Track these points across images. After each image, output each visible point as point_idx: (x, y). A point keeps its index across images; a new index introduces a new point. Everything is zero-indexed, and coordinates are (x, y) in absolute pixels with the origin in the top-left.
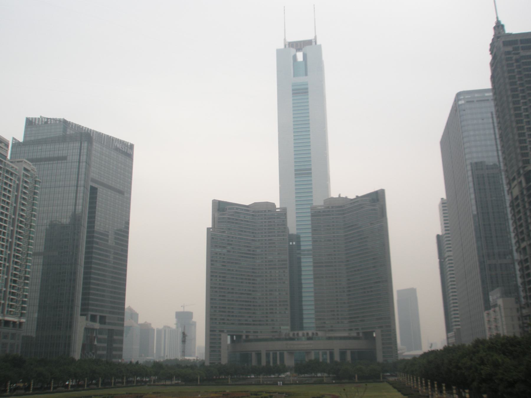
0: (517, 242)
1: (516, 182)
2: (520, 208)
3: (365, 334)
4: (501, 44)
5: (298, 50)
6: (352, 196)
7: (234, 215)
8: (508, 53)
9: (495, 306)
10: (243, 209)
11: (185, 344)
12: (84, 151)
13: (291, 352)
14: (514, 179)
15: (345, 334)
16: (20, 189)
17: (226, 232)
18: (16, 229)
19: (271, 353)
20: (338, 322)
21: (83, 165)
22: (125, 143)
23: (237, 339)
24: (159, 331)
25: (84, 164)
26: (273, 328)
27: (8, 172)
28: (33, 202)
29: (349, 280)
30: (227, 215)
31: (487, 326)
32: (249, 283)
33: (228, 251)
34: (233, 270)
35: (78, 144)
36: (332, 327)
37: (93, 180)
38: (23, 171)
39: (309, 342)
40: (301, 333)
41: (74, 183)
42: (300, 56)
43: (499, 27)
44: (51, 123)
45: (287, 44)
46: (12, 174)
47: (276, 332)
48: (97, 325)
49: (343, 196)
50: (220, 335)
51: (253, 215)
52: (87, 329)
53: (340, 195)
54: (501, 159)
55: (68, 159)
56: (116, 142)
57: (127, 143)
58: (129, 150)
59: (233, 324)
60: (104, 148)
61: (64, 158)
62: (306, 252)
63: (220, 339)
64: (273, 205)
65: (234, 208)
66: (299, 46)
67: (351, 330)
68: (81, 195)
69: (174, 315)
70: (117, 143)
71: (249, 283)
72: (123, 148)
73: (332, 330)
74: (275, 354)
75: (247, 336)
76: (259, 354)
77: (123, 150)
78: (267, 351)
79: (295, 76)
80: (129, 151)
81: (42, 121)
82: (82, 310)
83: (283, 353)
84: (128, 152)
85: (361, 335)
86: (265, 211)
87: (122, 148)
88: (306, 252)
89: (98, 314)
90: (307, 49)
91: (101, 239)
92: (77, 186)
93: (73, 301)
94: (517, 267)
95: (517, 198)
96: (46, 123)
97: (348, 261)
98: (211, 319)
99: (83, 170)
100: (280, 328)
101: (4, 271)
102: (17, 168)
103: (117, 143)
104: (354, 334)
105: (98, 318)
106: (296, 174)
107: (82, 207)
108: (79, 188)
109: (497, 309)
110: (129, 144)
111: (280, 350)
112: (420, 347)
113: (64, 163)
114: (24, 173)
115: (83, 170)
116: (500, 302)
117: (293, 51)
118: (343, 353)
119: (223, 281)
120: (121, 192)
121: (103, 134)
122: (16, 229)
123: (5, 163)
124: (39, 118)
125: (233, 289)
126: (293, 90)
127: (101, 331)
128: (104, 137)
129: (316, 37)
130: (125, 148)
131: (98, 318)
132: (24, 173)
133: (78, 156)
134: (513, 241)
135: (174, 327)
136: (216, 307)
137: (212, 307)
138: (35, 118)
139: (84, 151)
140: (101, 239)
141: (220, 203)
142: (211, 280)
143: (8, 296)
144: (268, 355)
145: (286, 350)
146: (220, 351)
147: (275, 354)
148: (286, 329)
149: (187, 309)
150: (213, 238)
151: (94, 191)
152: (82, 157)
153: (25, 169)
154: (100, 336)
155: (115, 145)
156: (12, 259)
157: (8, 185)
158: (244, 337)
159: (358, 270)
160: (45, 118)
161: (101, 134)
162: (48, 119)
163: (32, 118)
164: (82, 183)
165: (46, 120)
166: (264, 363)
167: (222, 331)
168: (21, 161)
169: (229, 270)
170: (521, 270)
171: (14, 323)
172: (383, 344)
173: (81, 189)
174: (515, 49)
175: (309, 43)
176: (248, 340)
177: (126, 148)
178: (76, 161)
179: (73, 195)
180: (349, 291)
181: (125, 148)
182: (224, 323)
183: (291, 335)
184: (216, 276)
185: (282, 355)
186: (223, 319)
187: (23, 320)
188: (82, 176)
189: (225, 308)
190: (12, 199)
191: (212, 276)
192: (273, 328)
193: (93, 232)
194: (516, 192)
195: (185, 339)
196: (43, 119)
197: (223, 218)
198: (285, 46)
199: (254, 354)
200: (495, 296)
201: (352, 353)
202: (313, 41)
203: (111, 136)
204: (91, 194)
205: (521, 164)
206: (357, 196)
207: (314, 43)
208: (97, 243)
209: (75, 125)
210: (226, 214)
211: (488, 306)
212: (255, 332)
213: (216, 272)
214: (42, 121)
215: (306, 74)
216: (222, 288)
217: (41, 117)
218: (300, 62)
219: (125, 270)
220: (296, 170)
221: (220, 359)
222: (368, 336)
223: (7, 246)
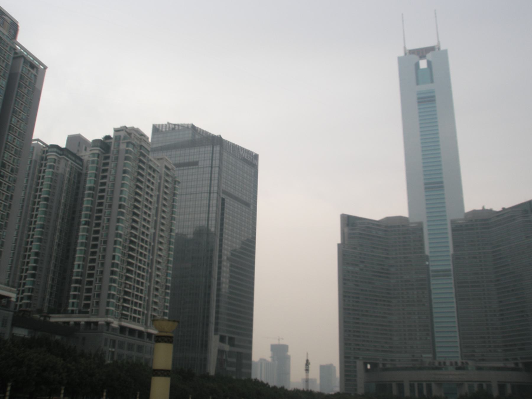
5: (422, 57)
6: (497, 208)
11: (308, 373)
12: (217, 155)
13: (439, 384)
15: (501, 364)
16: (162, 188)
19: (416, 384)
22: (250, 152)
25: (217, 169)
26: (413, 356)
27: (150, 168)
28: (172, 203)
29: (500, 302)
32: (384, 305)
33: (361, 270)
35: (209, 149)
37: (224, 192)
38: (164, 169)
39: (458, 372)
41: (207, 189)
42: (423, 64)
44: (179, 129)
45: (407, 52)
46: (154, 171)
48: (227, 347)
49: (487, 207)
50: (355, 362)
51: (385, 231)
52: (221, 352)
53: (483, 207)
55: (200, 164)
56: (241, 151)
57: (252, 153)
58: (254, 161)
60: (231, 157)
61: (195, 164)
62: (441, 273)
63: (355, 367)
66: (422, 53)
67: (506, 360)
69: (269, 348)
70: (242, 152)
71: (384, 305)
72: (248, 157)
73: (483, 360)
74: (420, 386)
75: (384, 365)
76: (400, 386)
77: (249, 160)
78: (410, 381)
79: (418, 83)
81: (169, 127)
84: (253, 162)
85: (521, 366)
87: (247, 157)
88: (441, 273)
90: (429, 56)
92: (210, 193)
96: (173, 129)
97: (498, 280)
98: (346, 344)
99: (215, 176)
100: (422, 356)
101: (147, 277)
102: (159, 164)
103: (242, 152)
104: (511, 365)
105: (227, 339)
106: (426, 188)
108: (212, 195)
110: (254, 154)
111: (418, 381)
113: (195, 168)
114: (165, 172)
115: (215, 176)
117: (415, 57)
118: (502, 386)
119: (357, 302)
120: (247, 205)
121: (229, 142)
123: (148, 158)
124: (166, 125)
125: (367, 311)
126: (419, 98)
128: (231, 145)
129: (439, 43)
130: (250, 158)
131: (227, 339)
132: (165, 172)
133: (211, 161)
135: (269, 359)
136: (350, 331)
137: (345, 331)
138: (162, 125)
139: (217, 155)
142: (344, 300)
144: (412, 386)
145: (433, 381)
147: (420, 386)
149: (282, 342)
150: (344, 255)
152: (214, 161)
153: (166, 168)
154: (229, 360)
155: (241, 154)
157: (151, 182)
158: (381, 366)
159: (513, 290)
160: (172, 124)
161: (228, 142)
162: (175, 125)
163: (159, 125)
165: (173, 126)
167: (356, 358)
168: (161, 159)
169: (362, 290)
175: (432, 49)
176: (385, 369)
177: (251, 158)
178: (208, 166)
179: (206, 202)
180: (502, 315)
181: (250, 158)
182: (359, 349)
184: (349, 297)
185: (429, 387)
186: (358, 345)
189: (359, 332)
190: (154, 199)
191: (344, 296)
192: (413, 356)
195: (308, 367)
196: (171, 126)
198: (406, 54)
202: (436, 47)
203: (236, 145)
207: (437, 50)
209: (203, 131)
212: (392, 360)
214: (169, 127)
215: (432, 81)
216: (356, 310)
217: (168, 123)
218: (423, 69)
219: (252, 289)
220: (426, 184)
221: (356, 390)
223: (149, 250)
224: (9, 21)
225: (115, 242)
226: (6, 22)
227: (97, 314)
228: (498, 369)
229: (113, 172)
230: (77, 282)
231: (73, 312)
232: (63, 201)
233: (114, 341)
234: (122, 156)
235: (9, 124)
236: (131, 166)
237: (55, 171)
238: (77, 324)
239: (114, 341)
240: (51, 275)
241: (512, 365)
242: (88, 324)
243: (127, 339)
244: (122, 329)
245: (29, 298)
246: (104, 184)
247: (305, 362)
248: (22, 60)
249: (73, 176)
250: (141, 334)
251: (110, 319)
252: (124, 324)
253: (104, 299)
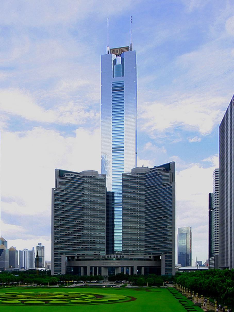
7: (69, 179)
10: (76, 175)
15: (142, 257)
17: (65, 191)
20: (137, 250)
30: (65, 179)
34: (69, 216)
36: (133, 252)
39: (118, 261)
47: (97, 255)
50: (61, 256)
53: (61, 174)
59: (69, 249)
63: (61, 259)
65: (70, 174)
74: (95, 269)
75: (78, 257)
76: (85, 269)
83: (101, 268)
85: (152, 258)
86: (91, 177)
96: (92, 172)
100: (99, 252)
104: (147, 257)
141: (60, 171)
144: (91, 269)
146: (60, 266)
147: (95, 269)
158: (76, 258)
166: (88, 274)
169: (66, 216)
172: (166, 263)
175: (127, 49)
176: (78, 260)
184: (58, 220)
185: (100, 269)
197: (63, 182)
206: (155, 167)
210: (64, 179)
213: (58, 217)
226: (185, 236)
241: (148, 257)
247: (100, 159)
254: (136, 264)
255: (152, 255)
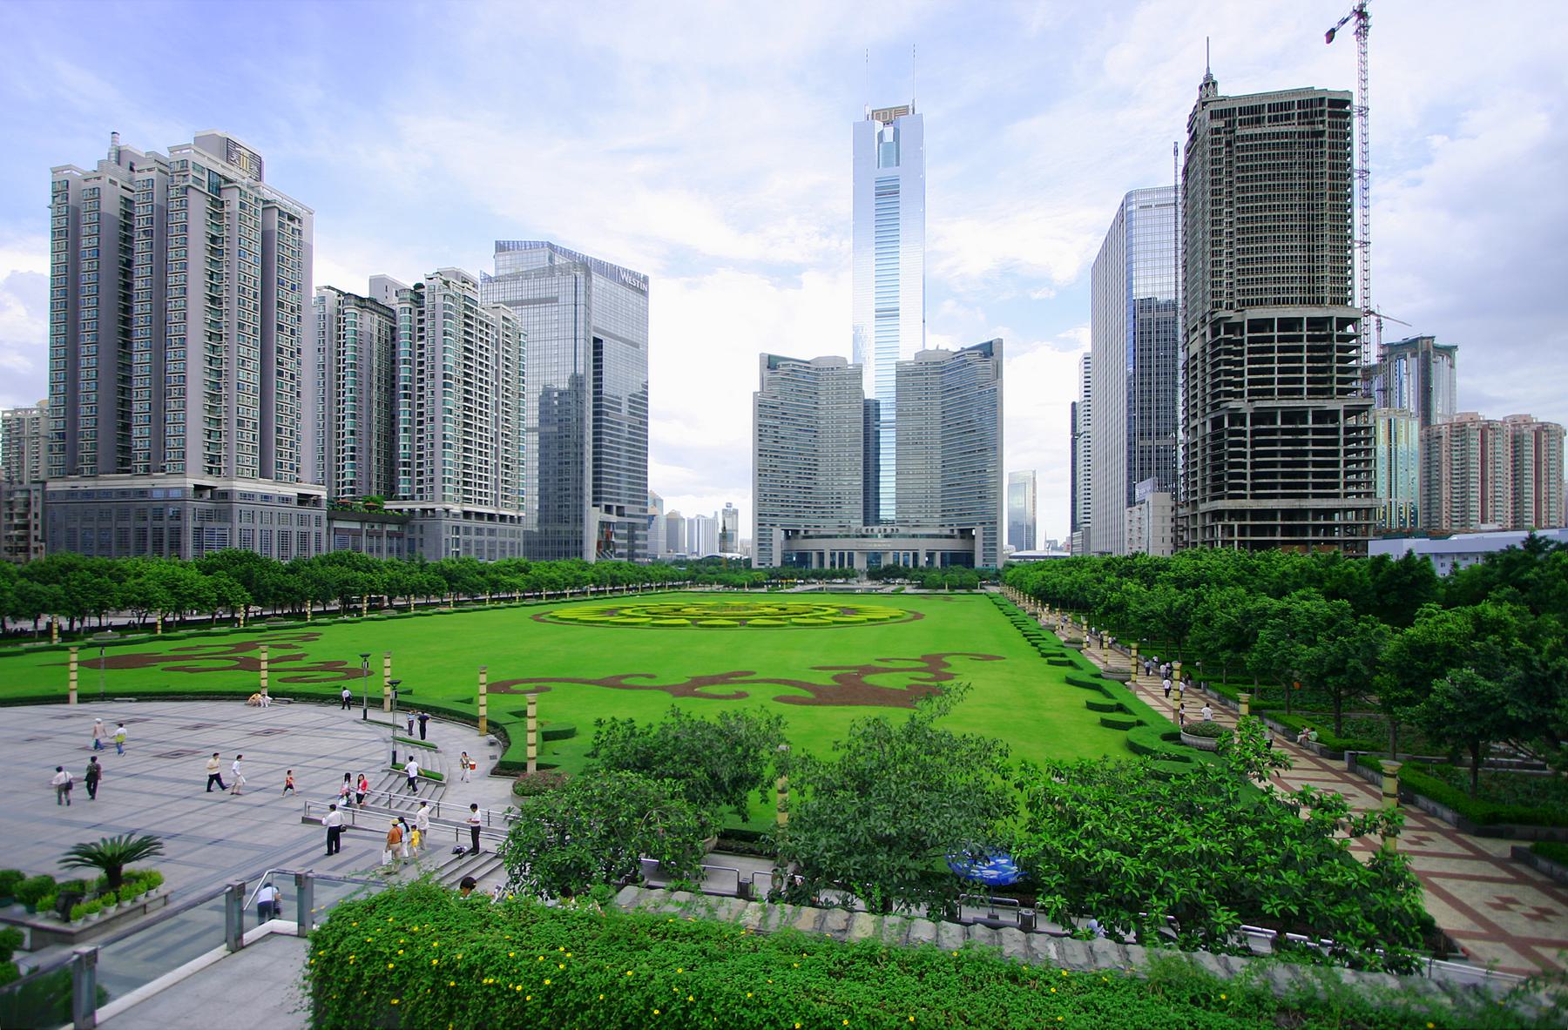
0: (1187, 418)
1: (1197, 334)
2: (1198, 381)
3: (961, 531)
4: (1208, 116)
8: (1217, 131)
9: (1142, 502)
14: (1195, 329)
15: (936, 531)
18: (501, 400)
21: (581, 309)
23: (791, 535)
24: (691, 522)
27: (481, 323)
31: (1127, 527)
37: (597, 330)
40: (876, 529)
43: (1209, 83)
48: (613, 518)
52: (603, 524)
54: (1180, 296)
61: (554, 300)
64: (844, 360)
66: (890, 116)
68: (581, 350)
74: (842, 555)
76: (821, 555)
80: (643, 287)
82: (595, 499)
85: (956, 532)
89: (615, 505)
91: (611, 408)
93: (582, 437)
94: (1181, 452)
95: (1195, 357)
99: (581, 316)
104: (946, 531)
107: (585, 367)
109: (1144, 506)
112: (1031, 545)
115: (581, 316)
116: (1149, 497)
120: (637, 346)
122: (501, 400)
127: (620, 525)
134: (1181, 417)
140: (611, 408)
143: (501, 485)
144: (833, 555)
147: (842, 555)
148: (857, 524)
151: (598, 343)
154: (618, 531)
156: (500, 438)
158: (802, 533)
164: (581, 334)
166: (827, 566)
170: (1186, 457)
171: (512, 517)
173: (581, 342)
174: (1228, 124)
175: (904, 110)
183: (864, 532)
185: (851, 556)
187: (521, 514)
188: (581, 325)
193: (601, 399)
194: (1195, 348)
199: (814, 553)
200: (1144, 489)
201: (942, 555)
204: (595, 347)
205: (1208, 308)
208: (607, 414)
211: (1131, 502)
215: (898, 164)
222: (966, 534)
224: (247, 154)
225: (444, 420)
227: (433, 499)
228: (929, 536)
229: (431, 333)
230: (405, 464)
231: (405, 498)
232: (375, 366)
233: (458, 528)
234: (439, 312)
235: (275, 299)
236: (455, 327)
237: (358, 329)
238: (412, 511)
239: (458, 528)
240: (375, 455)
241: (948, 532)
242: (424, 511)
243: (473, 523)
244: (467, 514)
245: (353, 491)
246: (422, 346)
248: (277, 212)
249: (383, 333)
250: (491, 517)
251: (447, 506)
252: (467, 508)
253: (438, 484)
254: (923, 546)
255: (956, 528)
